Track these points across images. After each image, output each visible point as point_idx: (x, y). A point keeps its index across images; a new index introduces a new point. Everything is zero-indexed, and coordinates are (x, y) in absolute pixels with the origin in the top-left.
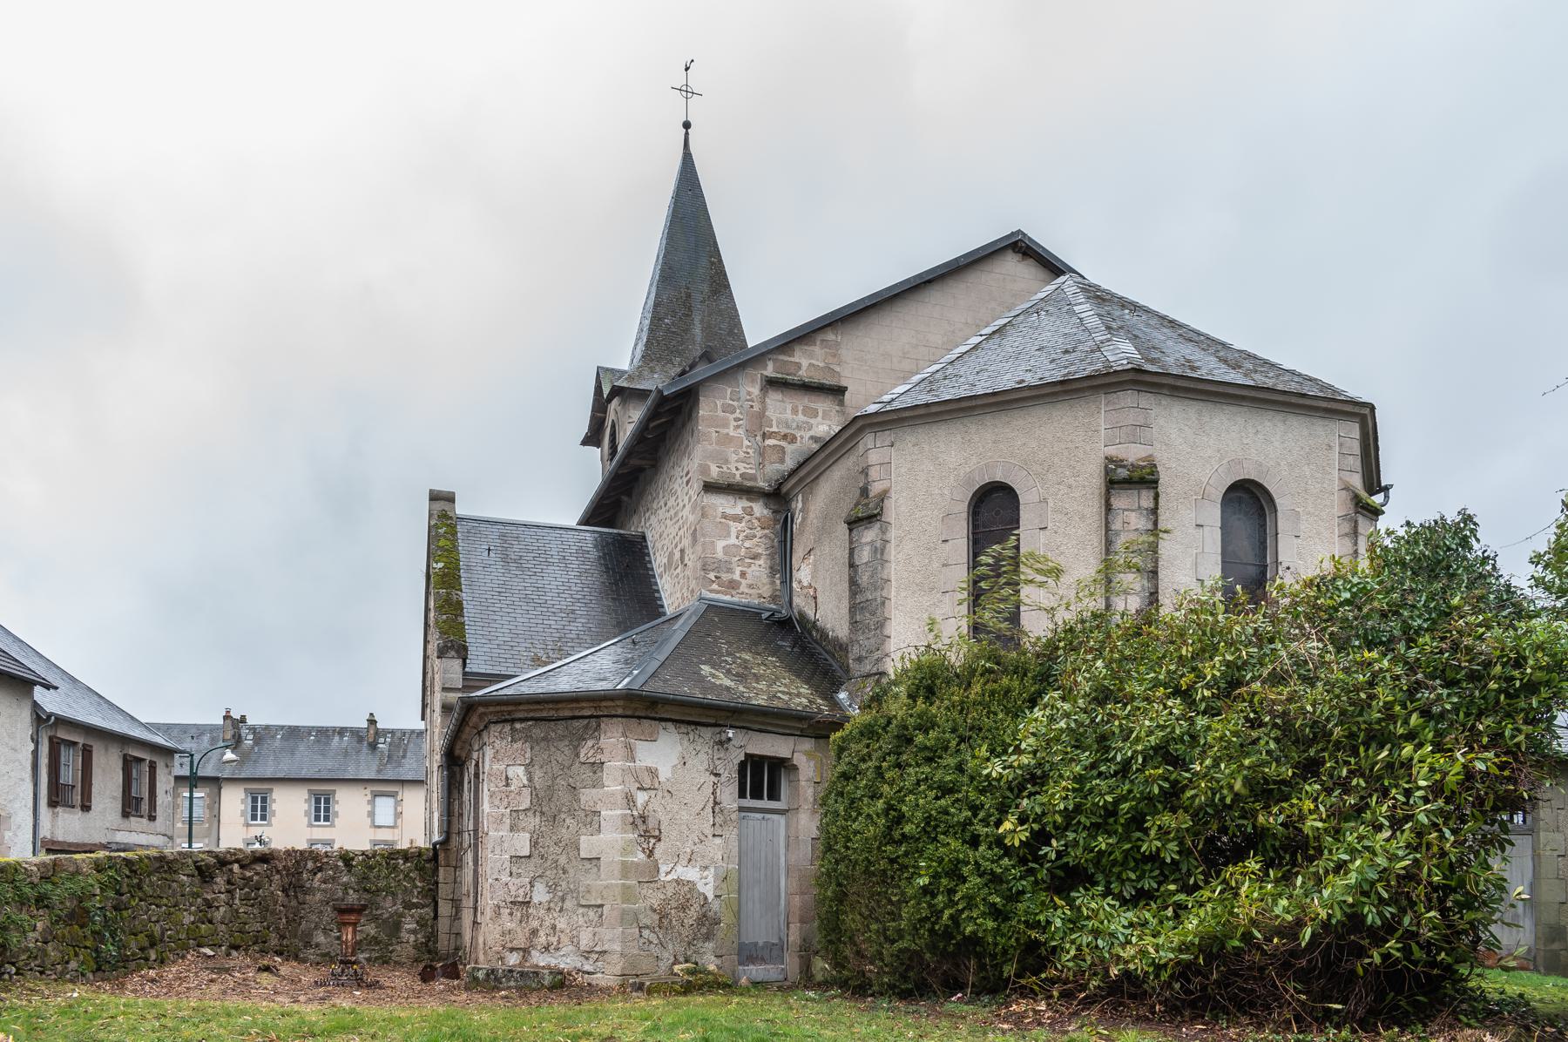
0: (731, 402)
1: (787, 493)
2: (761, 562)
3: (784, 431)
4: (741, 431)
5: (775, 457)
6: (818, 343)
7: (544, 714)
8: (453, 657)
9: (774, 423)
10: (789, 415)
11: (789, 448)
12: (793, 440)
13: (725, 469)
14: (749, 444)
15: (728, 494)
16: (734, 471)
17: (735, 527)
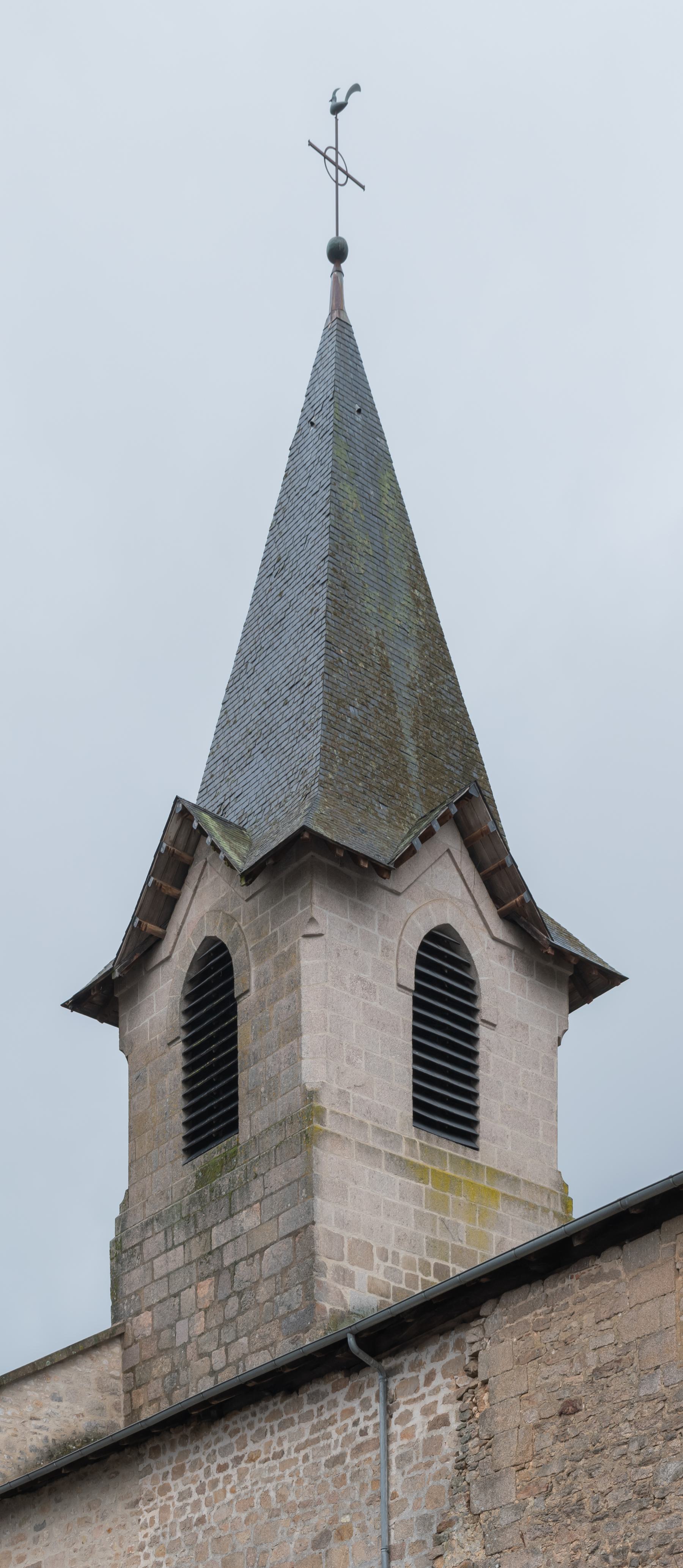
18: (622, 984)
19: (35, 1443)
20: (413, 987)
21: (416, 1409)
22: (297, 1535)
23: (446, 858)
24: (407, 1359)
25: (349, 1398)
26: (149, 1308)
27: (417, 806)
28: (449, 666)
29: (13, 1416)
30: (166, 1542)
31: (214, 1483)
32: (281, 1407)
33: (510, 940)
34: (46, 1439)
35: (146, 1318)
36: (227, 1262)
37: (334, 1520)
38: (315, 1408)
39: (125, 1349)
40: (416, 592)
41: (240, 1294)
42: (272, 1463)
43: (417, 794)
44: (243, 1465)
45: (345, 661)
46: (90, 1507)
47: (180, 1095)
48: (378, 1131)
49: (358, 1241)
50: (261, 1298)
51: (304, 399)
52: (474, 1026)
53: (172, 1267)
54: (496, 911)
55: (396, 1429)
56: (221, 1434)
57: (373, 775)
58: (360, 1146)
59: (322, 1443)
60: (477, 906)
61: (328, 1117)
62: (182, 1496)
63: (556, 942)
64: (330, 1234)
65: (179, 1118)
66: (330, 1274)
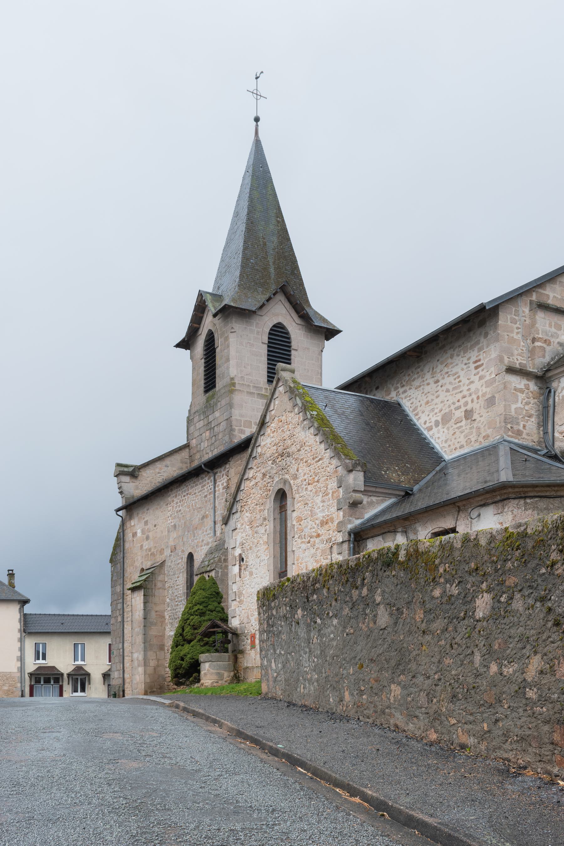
0: (514, 317)
1: (550, 377)
2: (533, 419)
3: (546, 337)
4: (520, 336)
5: (541, 354)
6: (558, 283)
7: (548, 494)
8: (360, 471)
9: (540, 332)
10: (547, 328)
11: (548, 349)
12: (549, 344)
13: (511, 360)
14: (524, 344)
15: (518, 375)
16: (516, 361)
17: (521, 396)
18: (336, 337)
19: (159, 480)
20: (267, 343)
21: (220, 483)
22: (198, 516)
23: (280, 302)
24: (219, 470)
25: (208, 479)
26: (195, 438)
27: (273, 286)
28: (288, 239)
29: (152, 473)
30: (173, 516)
31: (183, 500)
32: (196, 480)
33: (303, 323)
34: (163, 479)
35: (194, 441)
36: (212, 427)
37: (205, 513)
38: (202, 481)
39: (190, 450)
40: (278, 219)
41: (215, 436)
42: (194, 496)
43: (273, 282)
44: (188, 496)
45: (250, 246)
46: (158, 505)
47: (203, 375)
48: (254, 387)
49: (246, 421)
50: (220, 438)
51: (247, 163)
52: (290, 351)
53: (200, 426)
54: (297, 316)
55: (217, 489)
56: (184, 486)
57: (258, 279)
58: (248, 392)
59: (203, 491)
60: (291, 315)
61: (237, 385)
62: (177, 503)
63: (316, 324)
64: (237, 419)
65: (203, 382)
66: (236, 431)
